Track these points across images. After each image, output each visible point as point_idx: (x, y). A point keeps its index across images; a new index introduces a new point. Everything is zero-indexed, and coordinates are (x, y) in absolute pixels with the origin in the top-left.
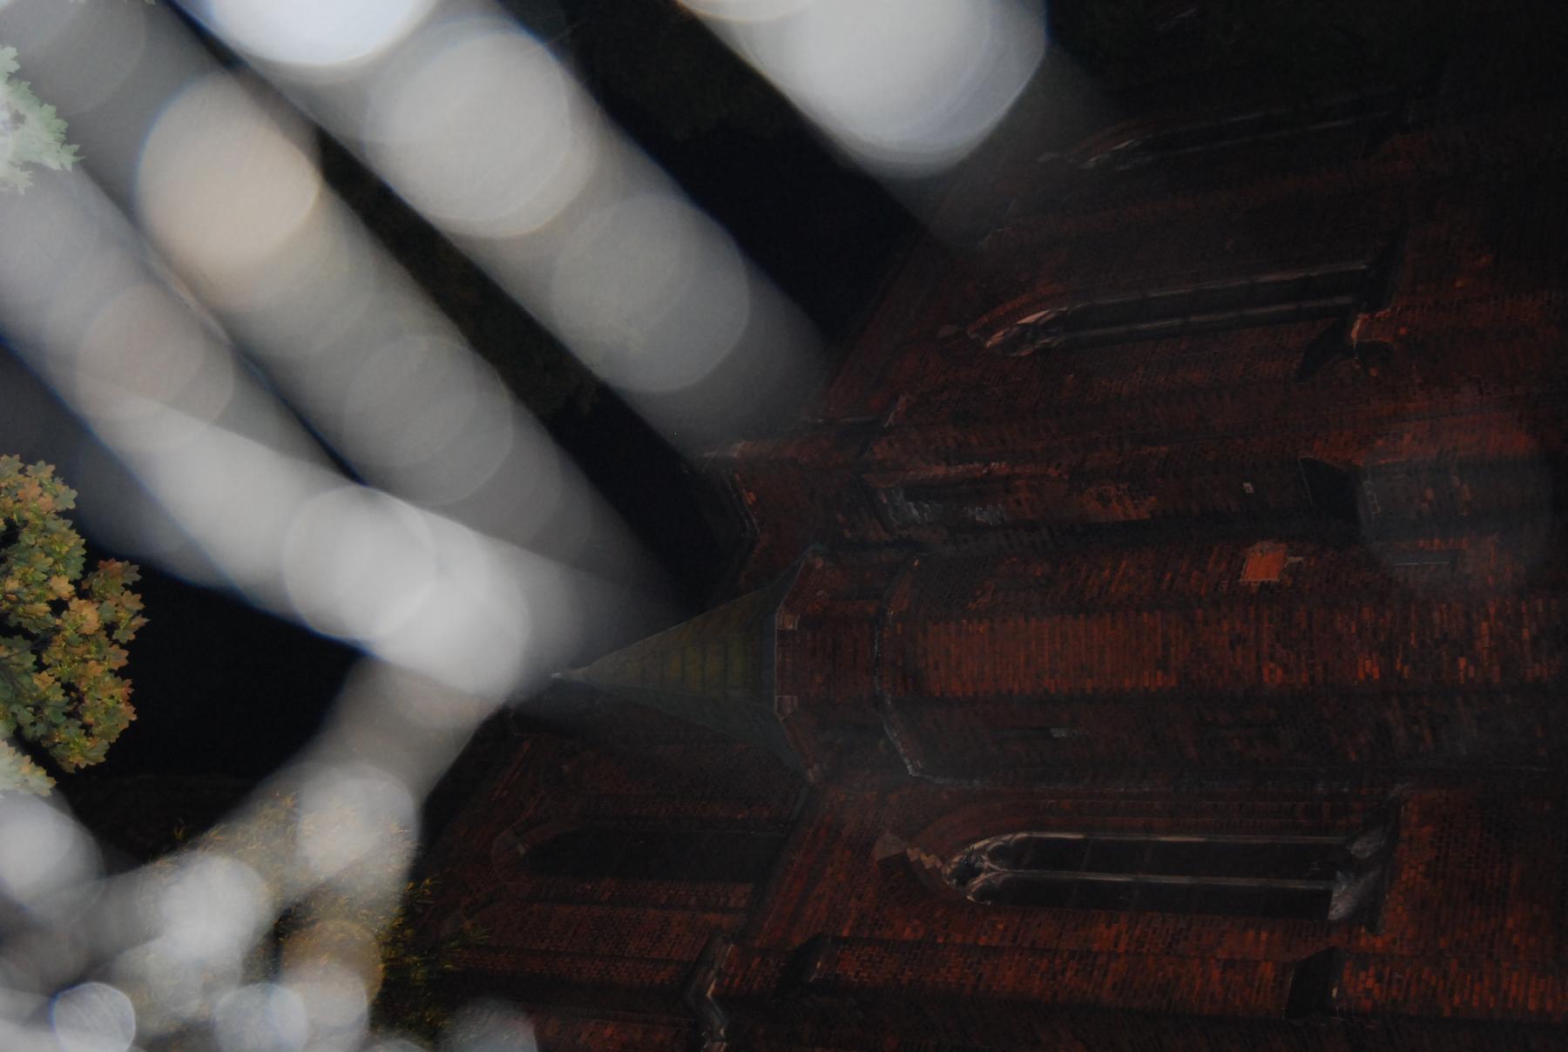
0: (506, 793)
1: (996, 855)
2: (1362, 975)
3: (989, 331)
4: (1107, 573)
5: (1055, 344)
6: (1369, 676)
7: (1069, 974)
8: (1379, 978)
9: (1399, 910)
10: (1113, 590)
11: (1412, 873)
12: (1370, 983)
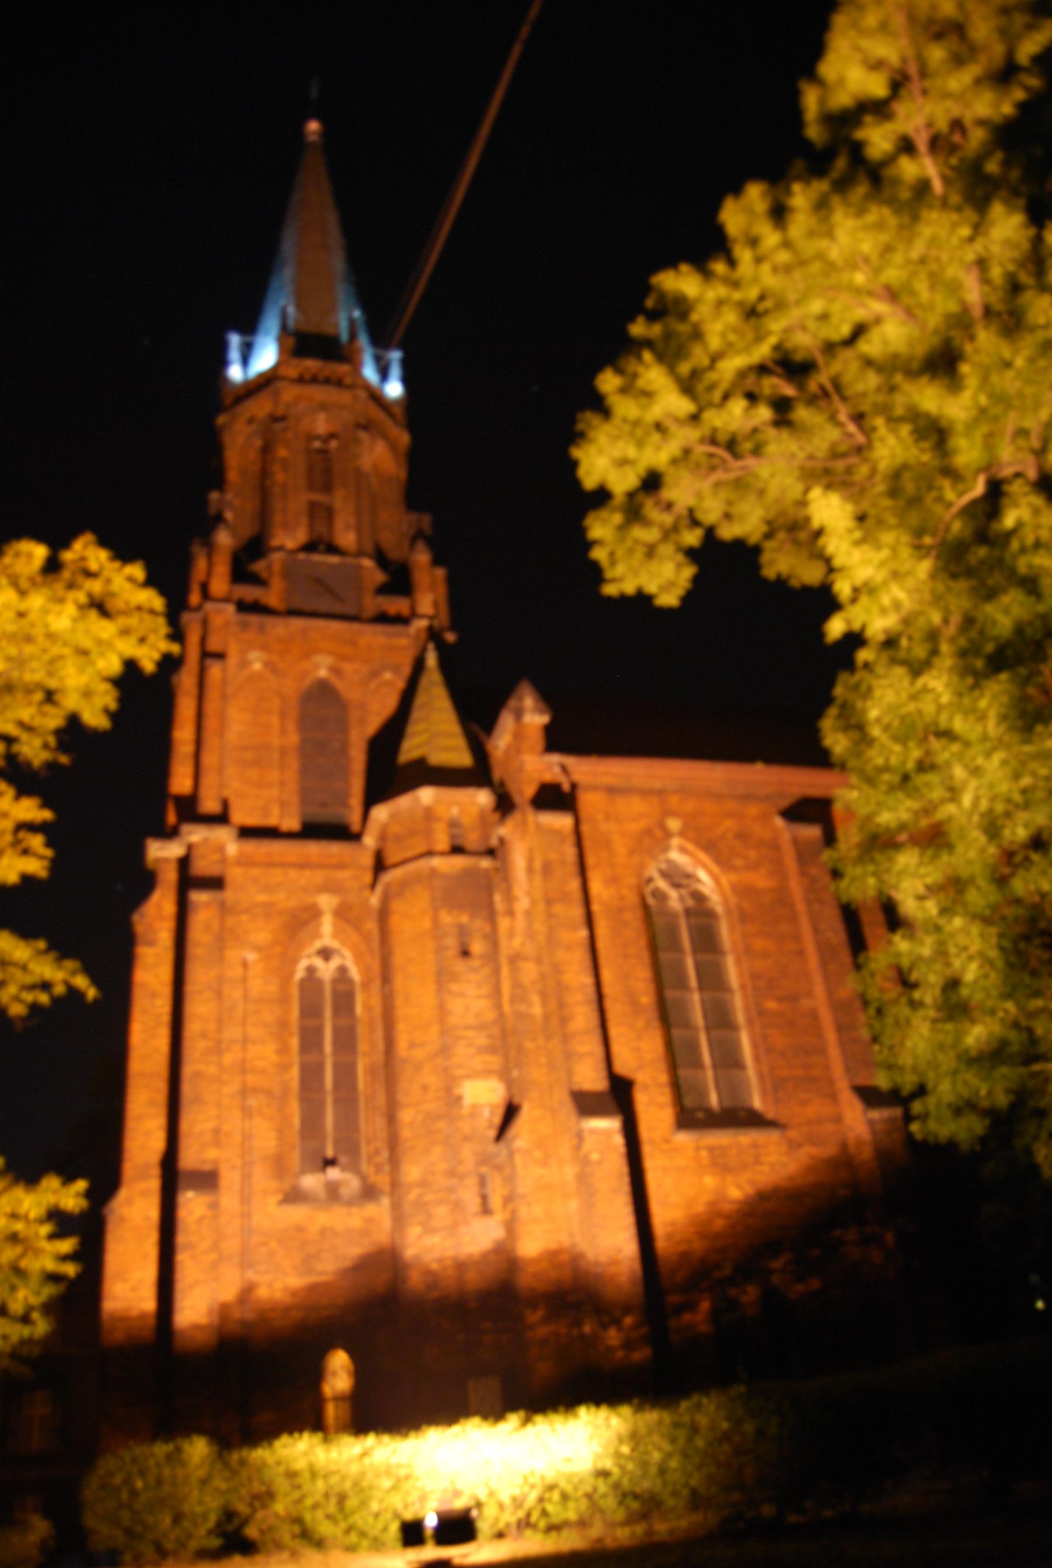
1: (343, 970)
3: (683, 850)
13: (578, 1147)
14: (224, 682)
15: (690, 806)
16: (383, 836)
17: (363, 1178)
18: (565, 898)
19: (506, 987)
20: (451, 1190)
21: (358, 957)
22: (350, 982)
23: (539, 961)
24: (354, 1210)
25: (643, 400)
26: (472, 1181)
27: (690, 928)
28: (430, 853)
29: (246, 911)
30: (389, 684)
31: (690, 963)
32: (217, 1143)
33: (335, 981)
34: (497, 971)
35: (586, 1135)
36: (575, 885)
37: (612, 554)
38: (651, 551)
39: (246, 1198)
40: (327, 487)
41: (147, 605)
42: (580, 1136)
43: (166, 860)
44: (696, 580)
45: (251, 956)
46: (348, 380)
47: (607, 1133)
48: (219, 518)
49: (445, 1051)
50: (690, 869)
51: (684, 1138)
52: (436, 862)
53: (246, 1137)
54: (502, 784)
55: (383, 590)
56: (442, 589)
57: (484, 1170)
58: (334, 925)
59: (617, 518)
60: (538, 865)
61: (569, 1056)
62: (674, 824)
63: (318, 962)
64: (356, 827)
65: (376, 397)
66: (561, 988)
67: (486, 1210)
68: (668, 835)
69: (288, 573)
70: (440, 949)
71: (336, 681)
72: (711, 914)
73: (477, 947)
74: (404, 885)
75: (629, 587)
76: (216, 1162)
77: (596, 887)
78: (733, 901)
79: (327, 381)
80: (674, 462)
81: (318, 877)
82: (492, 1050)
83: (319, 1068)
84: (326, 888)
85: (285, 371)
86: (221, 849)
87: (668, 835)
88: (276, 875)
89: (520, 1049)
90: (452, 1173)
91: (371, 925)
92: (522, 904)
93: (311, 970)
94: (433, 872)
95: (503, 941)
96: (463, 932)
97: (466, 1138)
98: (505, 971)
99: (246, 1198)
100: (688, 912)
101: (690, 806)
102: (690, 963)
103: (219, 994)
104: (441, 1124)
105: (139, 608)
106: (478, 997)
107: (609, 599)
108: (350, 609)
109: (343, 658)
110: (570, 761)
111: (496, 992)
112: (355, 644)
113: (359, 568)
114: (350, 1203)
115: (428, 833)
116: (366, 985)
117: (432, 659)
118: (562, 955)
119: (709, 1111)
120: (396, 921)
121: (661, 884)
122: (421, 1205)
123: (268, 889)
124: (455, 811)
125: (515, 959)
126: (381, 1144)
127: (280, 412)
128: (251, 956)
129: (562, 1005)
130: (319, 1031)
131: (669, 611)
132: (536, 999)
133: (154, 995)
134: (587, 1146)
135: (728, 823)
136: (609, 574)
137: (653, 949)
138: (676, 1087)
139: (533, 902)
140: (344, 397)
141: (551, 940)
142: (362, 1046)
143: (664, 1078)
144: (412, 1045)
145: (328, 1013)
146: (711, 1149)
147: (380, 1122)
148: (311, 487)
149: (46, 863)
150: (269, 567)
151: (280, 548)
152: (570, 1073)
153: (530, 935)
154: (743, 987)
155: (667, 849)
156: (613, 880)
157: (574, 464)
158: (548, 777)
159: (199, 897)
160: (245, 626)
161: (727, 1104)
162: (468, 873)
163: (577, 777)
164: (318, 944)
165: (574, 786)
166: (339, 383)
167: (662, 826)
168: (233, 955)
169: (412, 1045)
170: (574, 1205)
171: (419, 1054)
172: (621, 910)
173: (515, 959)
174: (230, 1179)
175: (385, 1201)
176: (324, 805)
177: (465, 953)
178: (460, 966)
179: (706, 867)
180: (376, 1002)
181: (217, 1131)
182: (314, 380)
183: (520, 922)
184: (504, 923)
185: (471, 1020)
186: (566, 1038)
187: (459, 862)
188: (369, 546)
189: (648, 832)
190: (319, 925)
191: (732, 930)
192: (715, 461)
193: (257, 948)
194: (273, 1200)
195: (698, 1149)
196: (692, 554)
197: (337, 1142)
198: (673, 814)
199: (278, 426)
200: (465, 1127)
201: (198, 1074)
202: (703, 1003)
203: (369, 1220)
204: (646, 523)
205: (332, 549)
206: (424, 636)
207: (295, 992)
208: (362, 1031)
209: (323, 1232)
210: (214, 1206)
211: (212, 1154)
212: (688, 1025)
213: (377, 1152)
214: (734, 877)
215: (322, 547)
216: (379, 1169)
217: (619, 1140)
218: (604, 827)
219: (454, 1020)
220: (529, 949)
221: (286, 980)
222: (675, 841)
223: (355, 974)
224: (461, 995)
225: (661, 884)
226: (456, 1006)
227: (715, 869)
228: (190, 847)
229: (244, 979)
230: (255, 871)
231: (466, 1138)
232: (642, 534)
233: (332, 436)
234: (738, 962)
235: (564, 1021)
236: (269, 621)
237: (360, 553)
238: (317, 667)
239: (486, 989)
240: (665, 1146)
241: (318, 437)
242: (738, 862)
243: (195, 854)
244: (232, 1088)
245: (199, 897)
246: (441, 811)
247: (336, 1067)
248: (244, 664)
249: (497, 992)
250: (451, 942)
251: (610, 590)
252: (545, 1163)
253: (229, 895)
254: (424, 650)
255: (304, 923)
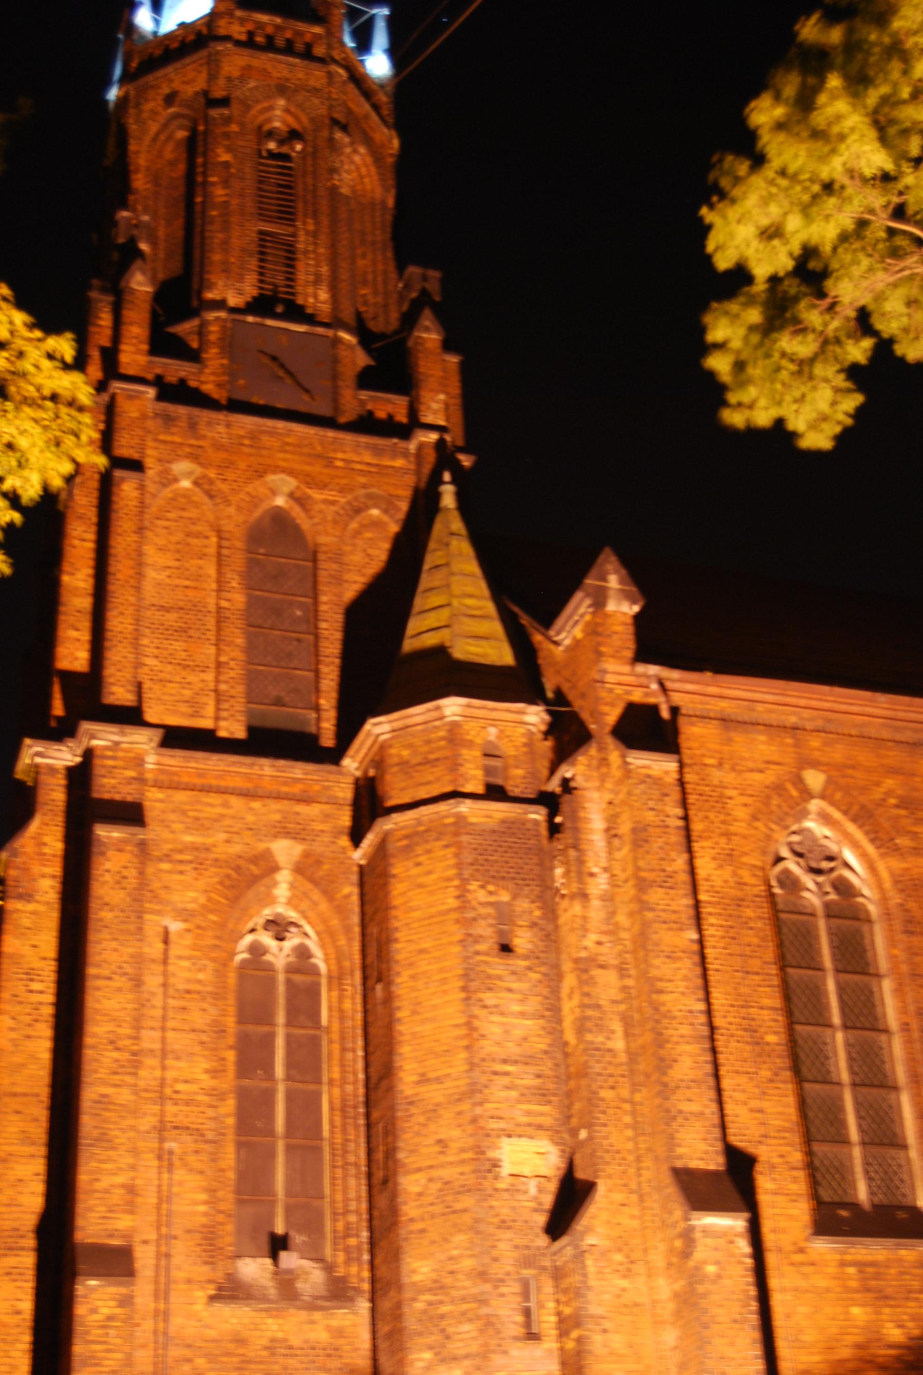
0: (339, 464)
1: (303, 953)
2: (112, 1303)
3: (825, 818)
4: (516, 1008)
5: (806, 894)
6: (414, 1271)
7: (116, 1055)
8: (110, 1318)
9: (235, 1321)
10: (495, 1018)
11: (275, 1327)
12: (105, 1311)
13: (686, 1254)
14: (142, 505)
15: (838, 753)
16: (379, 761)
17: (329, 1268)
18: (667, 882)
19: (569, 1008)
20: (482, 1301)
21: (327, 936)
22: (314, 971)
23: (622, 971)
24: (317, 1315)
25: (821, 147)
26: (512, 1288)
27: (831, 933)
28: (456, 795)
29: (167, 858)
30: (376, 524)
31: (831, 986)
32: (131, 1208)
33: (290, 969)
34: (554, 978)
35: (698, 1235)
36: (680, 862)
37: (739, 366)
38: (804, 367)
39: (162, 1292)
40: (287, 215)
41: (66, 394)
42: (688, 1236)
43: (52, 770)
44: (859, 413)
45: (175, 926)
46: (319, 50)
47: (723, 1234)
48: (131, 253)
49: (473, 1091)
50: (833, 847)
51: (823, 1246)
52: (465, 807)
53: (164, 1198)
54: (560, 698)
55: (366, 380)
56: (455, 387)
57: (526, 1272)
58: (292, 886)
59: (754, 316)
60: (625, 828)
61: (670, 1117)
62: (815, 779)
63: (267, 939)
64: (328, 740)
65: (358, 79)
66: (659, 1015)
67: (532, 1336)
68: (807, 794)
69: (229, 346)
70: (470, 939)
71: (297, 513)
72: (859, 916)
73: (522, 941)
74: (414, 837)
75: (763, 418)
76: (128, 1235)
77: (704, 866)
78: (896, 899)
79: (289, 49)
80: (844, 238)
81: (273, 811)
82: (542, 1095)
83: (268, 1097)
84: (283, 831)
85: (223, 27)
86: (139, 761)
87: (807, 794)
88: (212, 805)
89: (593, 1100)
90: (482, 1275)
91: (350, 890)
92: (599, 884)
93: (257, 950)
94: (460, 819)
95: (570, 938)
96: (504, 915)
97: (503, 1225)
98: (569, 981)
99: (162, 1292)
100: (831, 912)
101: (838, 753)
102: (831, 986)
103: (137, 982)
104: (467, 1201)
105: (54, 397)
106: (522, 1015)
107: (732, 433)
108: (322, 408)
109: (310, 481)
110: (672, 675)
111: (553, 1011)
112: (329, 463)
113: (337, 341)
114: (312, 1307)
115: (454, 766)
116: (336, 979)
117: (448, 496)
118: (661, 967)
119: (854, 1206)
120: (399, 891)
121: (792, 865)
122: (432, 1318)
123: (199, 825)
124: (492, 733)
125: (585, 966)
126: (357, 1218)
127: (218, 93)
128: (175, 926)
129: (660, 1041)
130: (268, 1041)
131: (816, 455)
132: (617, 1027)
133: (31, 975)
134: (699, 1254)
135: (889, 783)
136: (732, 398)
137: (783, 963)
138: (812, 1168)
139: (613, 881)
140: (316, 76)
141: (642, 941)
142: (331, 1071)
143: (797, 1157)
144: (423, 1080)
145: (281, 1018)
146: (861, 1265)
147: (357, 1187)
148: (263, 216)
149: (783, 1036)
150: (201, 332)
151: (220, 304)
152: (671, 1142)
153: (613, 932)
154: (905, 1027)
155: (804, 814)
156: (729, 858)
157: (705, 229)
158: (637, 696)
159: (106, 833)
160: (168, 420)
161: (880, 1198)
162: (509, 827)
163: (677, 699)
164: (268, 912)
165: (675, 711)
166: (307, 54)
167: (799, 781)
168: (154, 923)
169: (423, 1080)
170: (670, 1336)
171: (434, 1094)
172: (739, 902)
173: (585, 966)
174: (144, 1258)
175: (364, 1305)
176: (278, 702)
177: (506, 948)
178: (498, 966)
179: (855, 845)
180: (353, 1005)
181: (131, 1190)
182: (270, 46)
183: (596, 911)
184: (570, 911)
185: (512, 1049)
186: (665, 1091)
187: (499, 810)
188: (348, 315)
189: (778, 788)
190: (275, 884)
191: (891, 942)
192: (900, 241)
193: (184, 915)
194: (201, 1295)
195: (843, 1264)
196: (854, 372)
197: (289, 1210)
198: (814, 764)
199: (215, 113)
200: (502, 1207)
201: (104, 1101)
202: (848, 1044)
203: (339, 1333)
204: (801, 330)
205: (296, 313)
206: (430, 458)
207: (232, 979)
208: (330, 1048)
209: (273, 1347)
210: (126, 1301)
211: (124, 1222)
212: (826, 1079)
213: (348, 1232)
214: (897, 864)
215: (280, 309)
216: (351, 1258)
217: (744, 1246)
218: (717, 776)
219: (487, 1047)
220: (608, 953)
221: (223, 964)
222: (815, 805)
223: (319, 960)
224: (498, 1010)
225: (792, 865)
226: (491, 1026)
227: (870, 849)
228: (89, 754)
229: (165, 961)
230: (181, 796)
231: (503, 1225)
232: (787, 343)
233: (294, 135)
234: (899, 990)
235: (663, 1064)
236: (205, 415)
237: (336, 323)
238: (274, 493)
239: (534, 1004)
240: (798, 1258)
241: (270, 134)
242: (903, 841)
243: (99, 765)
244: (147, 1122)
245: (106, 833)
246: (472, 731)
247: (290, 1097)
248: (168, 479)
249: (553, 1011)
250: (484, 929)
251: (735, 418)
252: (627, 1274)
253: (152, 832)
254: (435, 480)
255: (254, 880)
